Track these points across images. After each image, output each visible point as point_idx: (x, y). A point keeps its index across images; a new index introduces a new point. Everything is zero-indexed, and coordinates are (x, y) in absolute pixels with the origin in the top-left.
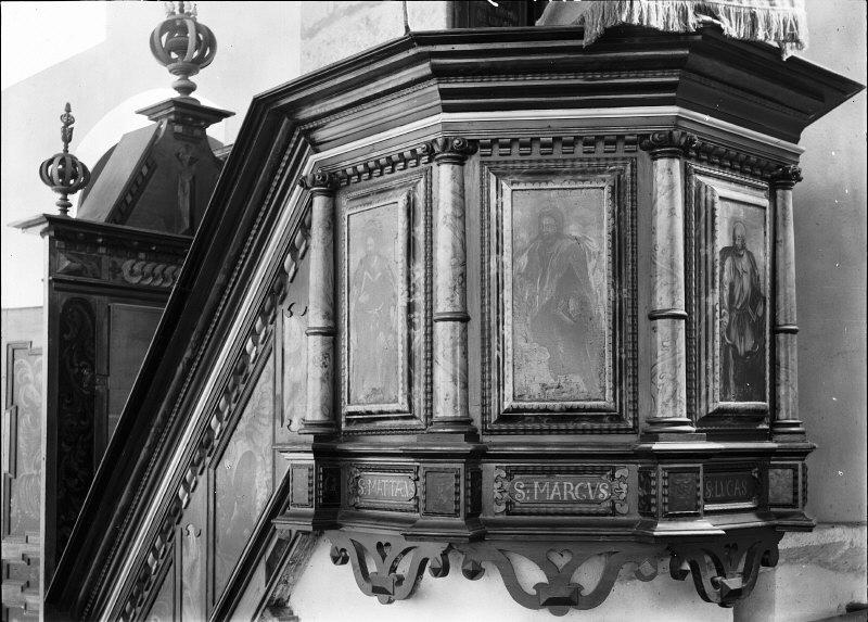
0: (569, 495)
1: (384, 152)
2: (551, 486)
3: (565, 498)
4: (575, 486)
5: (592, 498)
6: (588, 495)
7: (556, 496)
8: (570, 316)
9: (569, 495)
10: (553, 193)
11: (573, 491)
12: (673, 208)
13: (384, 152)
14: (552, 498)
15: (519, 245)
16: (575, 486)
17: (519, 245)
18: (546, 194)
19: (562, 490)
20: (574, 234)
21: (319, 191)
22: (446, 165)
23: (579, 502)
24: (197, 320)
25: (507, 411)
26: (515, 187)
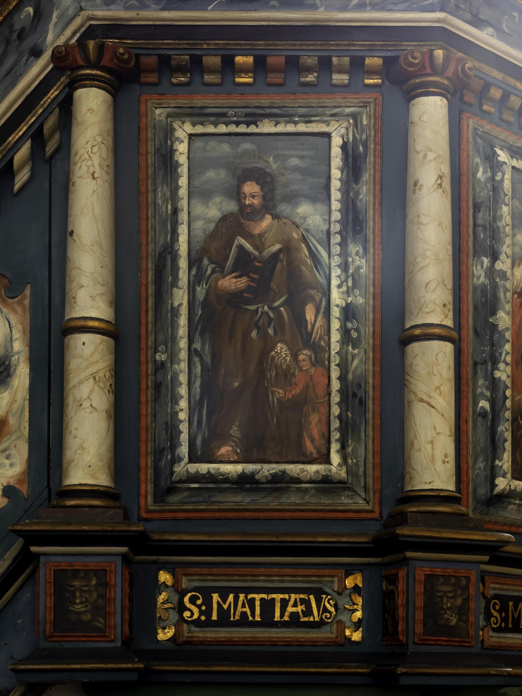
7: (244, 614)
14: (237, 617)
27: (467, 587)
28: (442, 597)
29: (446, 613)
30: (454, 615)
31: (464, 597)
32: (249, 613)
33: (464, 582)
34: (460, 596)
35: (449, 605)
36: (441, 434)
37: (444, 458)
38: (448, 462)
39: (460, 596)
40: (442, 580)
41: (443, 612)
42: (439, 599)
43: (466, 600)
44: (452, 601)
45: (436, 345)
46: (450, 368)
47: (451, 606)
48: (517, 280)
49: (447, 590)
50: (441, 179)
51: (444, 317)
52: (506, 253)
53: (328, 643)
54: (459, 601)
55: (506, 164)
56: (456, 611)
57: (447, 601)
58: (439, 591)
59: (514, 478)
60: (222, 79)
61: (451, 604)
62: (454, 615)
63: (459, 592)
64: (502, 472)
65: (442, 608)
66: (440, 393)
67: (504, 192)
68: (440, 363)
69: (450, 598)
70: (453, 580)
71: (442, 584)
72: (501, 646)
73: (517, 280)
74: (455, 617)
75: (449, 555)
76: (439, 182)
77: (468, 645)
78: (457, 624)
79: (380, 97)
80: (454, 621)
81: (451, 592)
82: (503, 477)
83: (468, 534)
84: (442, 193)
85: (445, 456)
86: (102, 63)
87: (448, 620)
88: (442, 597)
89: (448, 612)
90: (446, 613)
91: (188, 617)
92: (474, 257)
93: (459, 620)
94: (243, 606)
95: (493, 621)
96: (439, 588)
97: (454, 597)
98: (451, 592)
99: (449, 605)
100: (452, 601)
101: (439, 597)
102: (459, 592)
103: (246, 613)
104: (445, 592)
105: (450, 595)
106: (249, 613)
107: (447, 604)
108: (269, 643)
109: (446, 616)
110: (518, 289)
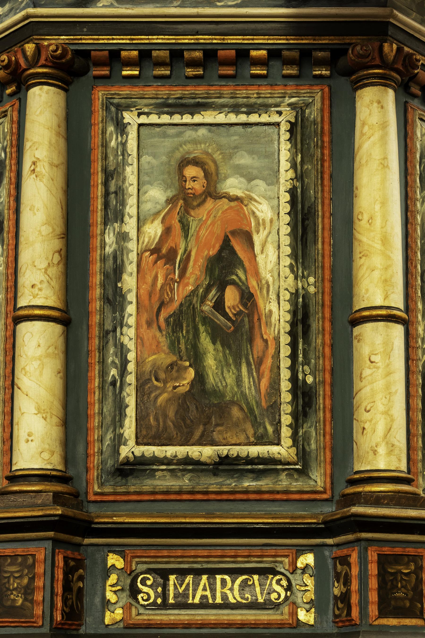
0: (224, 597)
1: (203, 39)
2: (196, 585)
3: (219, 600)
4: (233, 582)
5: (261, 600)
6: (10, 586)
7: (203, 597)
8: (229, 319)
9: (224, 597)
10: (202, 131)
11: (231, 589)
12: (385, 158)
13: (203, 39)
15: (147, 207)
16: (233, 582)
17: (147, 207)
18: (189, 134)
19: (213, 591)
20: (234, 192)
21: (394, 86)
22: (46, 88)
23: (238, 606)
24: (216, 322)
25: (127, 462)
26: (143, 119)
27: (33, 565)
28: (9, 578)
29: (12, 594)
30: (20, 595)
31: (30, 576)
32: (209, 596)
33: (30, 561)
34: (27, 575)
35: (15, 585)
36: (25, 414)
37: (27, 437)
38: (32, 441)
39: (27, 575)
40: (9, 561)
41: (9, 593)
42: (6, 580)
43: (32, 579)
44: (19, 581)
45: (38, 325)
46: (39, 346)
47: (17, 586)
48: (150, 237)
49: (14, 570)
50: (34, 164)
51: (32, 297)
52: (128, 213)
53: (281, 625)
54: (25, 581)
55: (130, 124)
56: (23, 591)
57: (14, 581)
58: (6, 572)
59: (138, 443)
60: (300, 70)
61: (18, 584)
62: (20, 595)
63: (26, 571)
64: (123, 440)
65: (8, 589)
66: (26, 373)
67: (128, 153)
68: (26, 344)
69: (16, 578)
70: (20, 559)
71: (9, 565)
72: (150, 624)
73: (150, 237)
74: (21, 597)
75: (13, 535)
76: (32, 168)
77: (35, 625)
78: (22, 604)
79: (18, 103)
80: (20, 601)
81: (17, 572)
82: (124, 445)
83: (15, 512)
84: (35, 178)
85: (29, 435)
86: (396, 66)
87: (14, 600)
88: (9, 578)
89: (14, 593)
90: (12, 594)
91: (276, 599)
92: (105, 224)
93: (25, 600)
94: (204, 589)
95: (142, 598)
96: (6, 569)
97: (21, 577)
98: (17, 572)
99: (15, 585)
100: (19, 581)
101: (6, 578)
102: (26, 571)
103: (206, 596)
104: (12, 573)
105: (17, 575)
106: (209, 596)
107: (14, 584)
108: (276, 626)
109: (12, 596)
110: (152, 246)
